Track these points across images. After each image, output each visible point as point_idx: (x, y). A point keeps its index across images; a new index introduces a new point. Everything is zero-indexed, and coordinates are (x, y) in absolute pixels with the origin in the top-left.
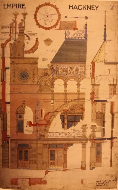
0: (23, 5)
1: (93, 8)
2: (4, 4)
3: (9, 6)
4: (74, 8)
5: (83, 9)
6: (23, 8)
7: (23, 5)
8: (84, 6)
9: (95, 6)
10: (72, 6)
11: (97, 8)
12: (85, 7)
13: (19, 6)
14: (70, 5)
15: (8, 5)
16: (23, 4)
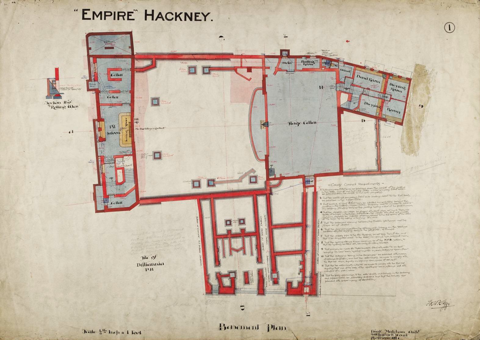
0: (197, 15)
1: (85, 15)
2: (84, 10)
3: (97, 16)
4: (158, 17)
5: (176, 20)
6: (128, 19)
7: (197, 15)
8: (177, 15)
9: (202, 13)
10: (152, 15)
11: (205, 16)
12: (179, 16)
13: (119, 16)
14: (146, 11)
15: (94, 13)
16: (128, 13)
